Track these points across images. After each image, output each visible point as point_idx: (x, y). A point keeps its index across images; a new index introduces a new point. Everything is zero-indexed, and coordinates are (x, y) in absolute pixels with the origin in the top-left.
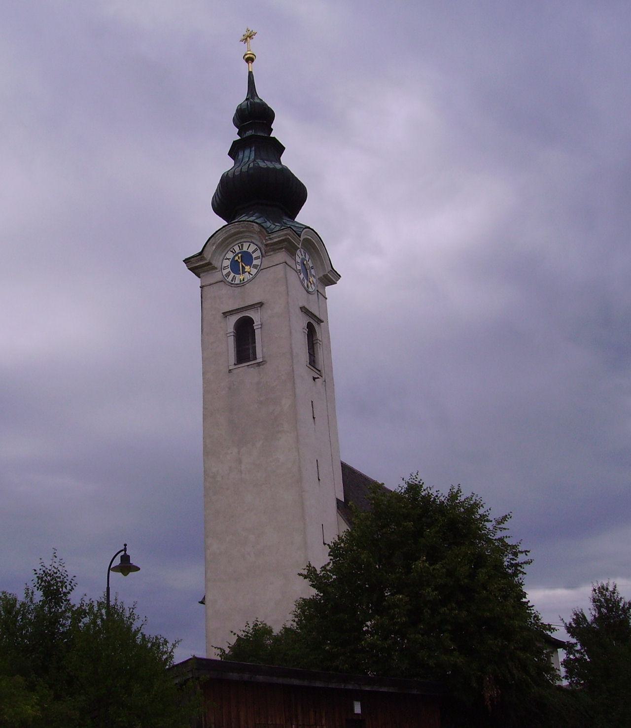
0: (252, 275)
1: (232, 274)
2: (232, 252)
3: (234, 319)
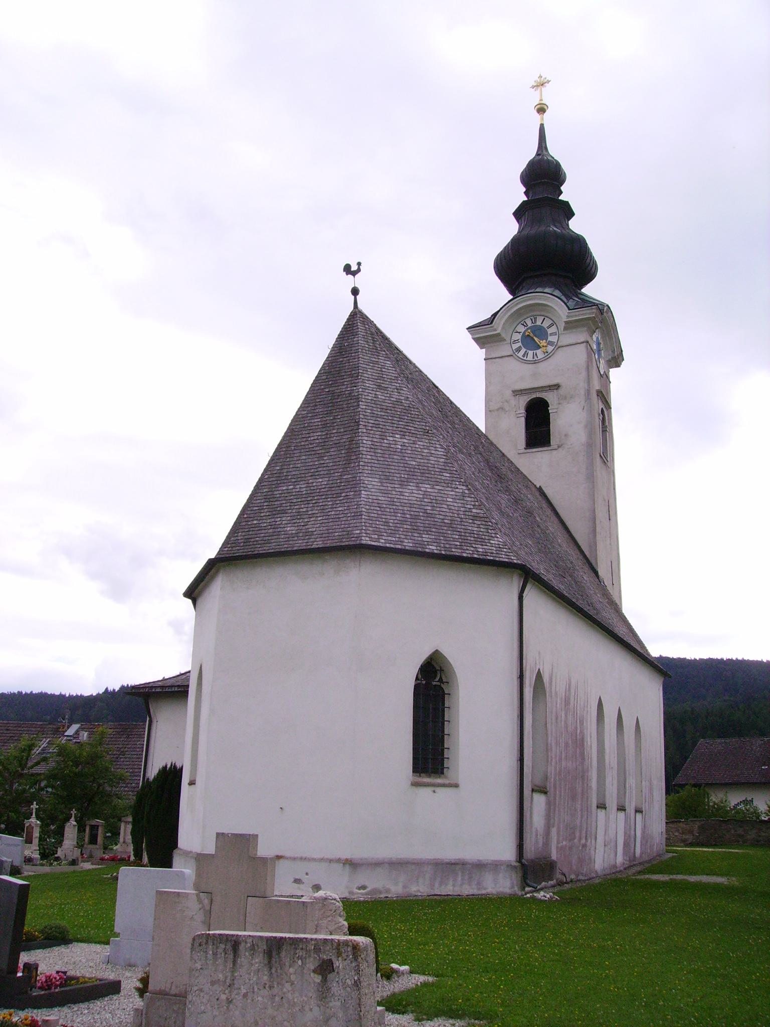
2: (523, 325)
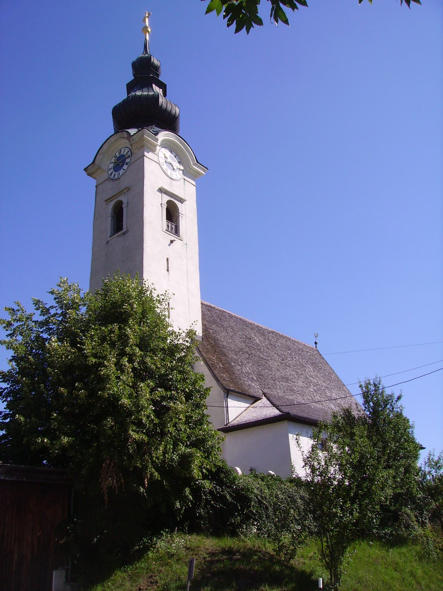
0: (124, 170)
1: (114, 173)
3: (112, 204)
